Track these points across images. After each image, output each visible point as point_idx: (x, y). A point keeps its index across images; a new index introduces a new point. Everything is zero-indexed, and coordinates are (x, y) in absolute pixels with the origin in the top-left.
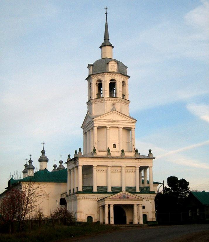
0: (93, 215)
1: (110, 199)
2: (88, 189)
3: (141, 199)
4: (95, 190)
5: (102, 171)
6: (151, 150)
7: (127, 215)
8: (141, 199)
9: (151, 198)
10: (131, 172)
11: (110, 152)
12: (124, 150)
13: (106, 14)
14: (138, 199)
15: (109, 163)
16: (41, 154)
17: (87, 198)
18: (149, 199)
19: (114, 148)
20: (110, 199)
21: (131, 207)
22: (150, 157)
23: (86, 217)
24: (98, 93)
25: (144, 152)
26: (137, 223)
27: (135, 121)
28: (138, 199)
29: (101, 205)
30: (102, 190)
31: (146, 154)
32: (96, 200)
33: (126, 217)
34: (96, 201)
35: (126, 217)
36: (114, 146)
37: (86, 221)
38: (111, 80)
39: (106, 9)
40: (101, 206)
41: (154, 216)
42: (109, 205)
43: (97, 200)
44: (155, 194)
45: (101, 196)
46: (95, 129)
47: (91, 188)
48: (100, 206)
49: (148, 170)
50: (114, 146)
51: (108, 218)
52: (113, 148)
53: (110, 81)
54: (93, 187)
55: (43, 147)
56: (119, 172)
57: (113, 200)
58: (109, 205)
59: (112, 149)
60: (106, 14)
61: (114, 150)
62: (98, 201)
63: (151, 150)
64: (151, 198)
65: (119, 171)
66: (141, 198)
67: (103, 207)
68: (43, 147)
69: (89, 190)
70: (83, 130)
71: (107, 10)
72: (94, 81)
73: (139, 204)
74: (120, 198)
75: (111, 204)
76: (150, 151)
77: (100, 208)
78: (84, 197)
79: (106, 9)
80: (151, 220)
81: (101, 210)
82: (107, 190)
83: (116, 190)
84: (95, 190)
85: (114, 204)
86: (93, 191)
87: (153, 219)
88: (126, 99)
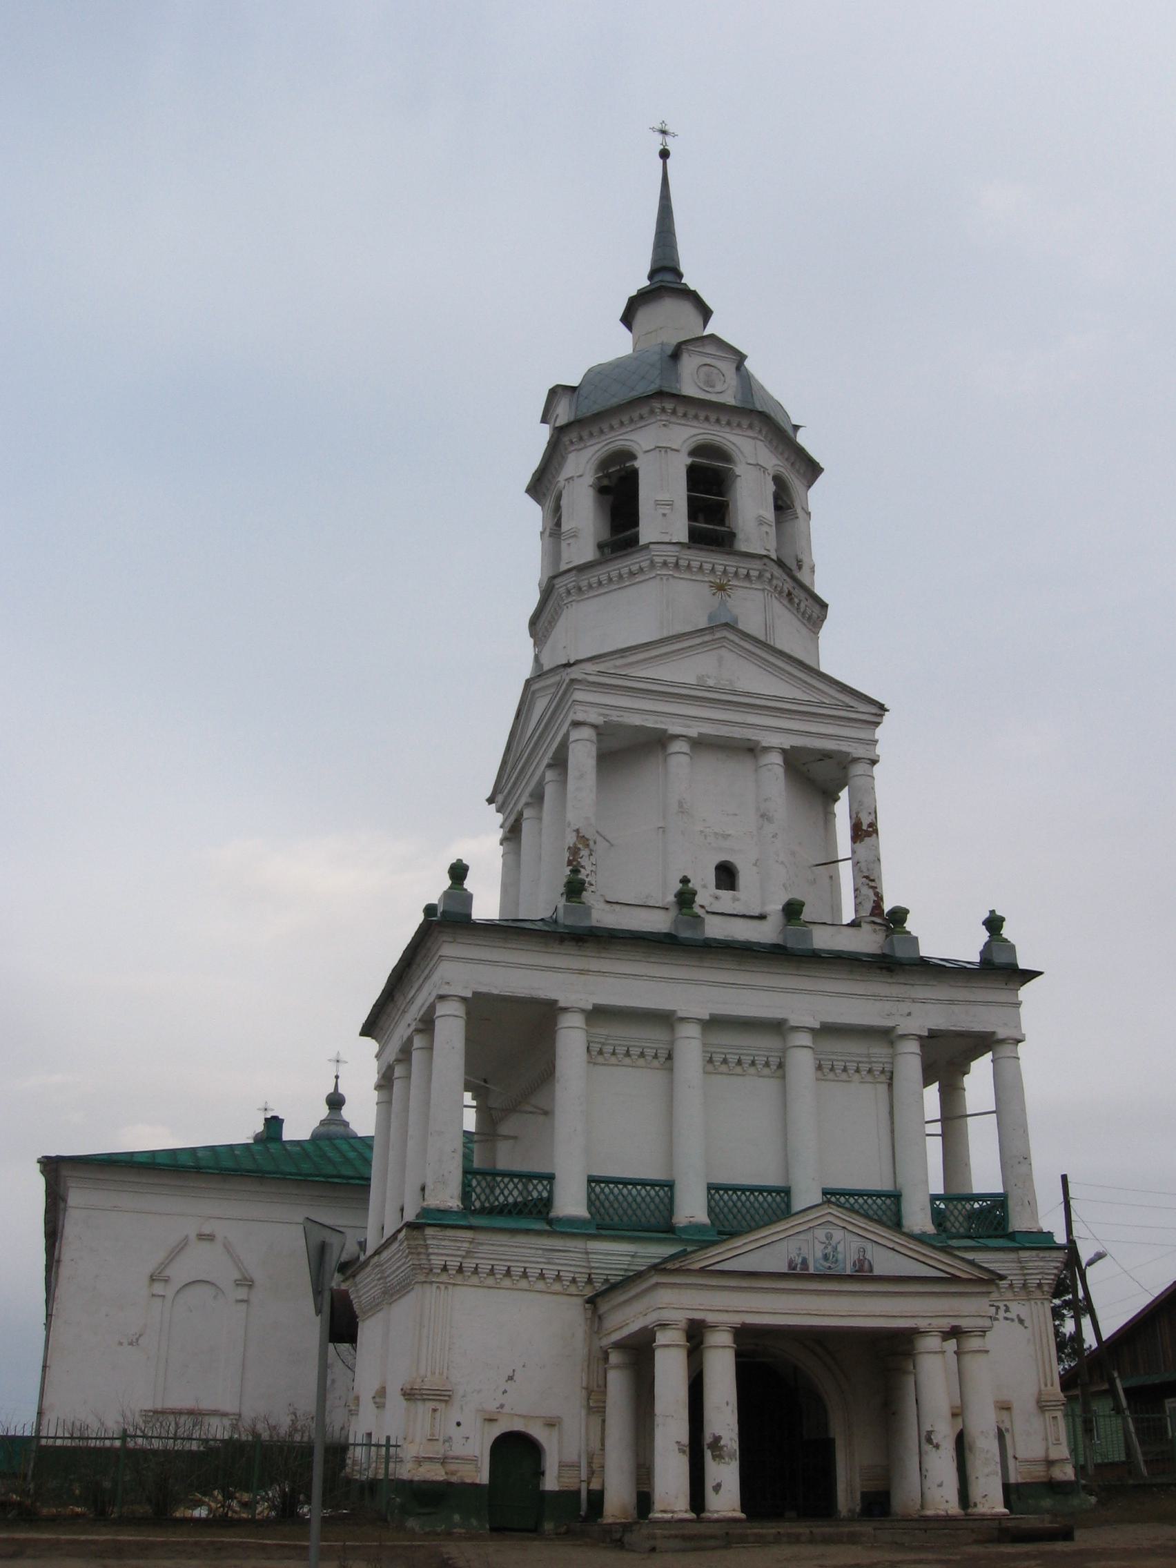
0: (551, 1424)
1: (703, 1271)
2: (511, 1193)
3: (980, 1281)
4: (571, 1202)
5: (628, 1054)
6: (1002, 919)
7: (837, 1431)
8: (980, 1281)
9: (1025, 1286)
10: (857, 1076)
11: (697, 909)
12: (802, 904)
13: (664, 154)
14: (954, 1279)
15: (693, 993)
16: (324, 1111)
17: (501, 1268)
18: (1009, 1295)
19: (726, 894)
20: (703, 1271)
21: (889, 1353)
22: (1000, 970)
23: (518, 1426)
24: (605, 535)
25: (947, 936)
26: (953, 1508)
27: (874, 710)
28: (954, 1279)
29: (616, 1337)
30: (633, 1209)
31: (967, 947)
32: (573, 1290)
33: (826, 1448)
34: (579, 1301)
35: (833, 1440)
36: (726, 875)
37: (484, 1477)
38: (696, 451)
39: (664, 132)
40: (618, 1345)
41: (1057, 1442)
42: (696, 1334)
43: (589, 1292)
44: (1055, 1254)
45: (615, 1255)
46: (583, 755)
47: (537, 1191)
48: (606, 1342)
49: (979, 1079)
50: (726, 875)
51: (681, 1456)
52: (720, 892)
53: (692, 453)
54: (551, 1178)
55: (337, 1077)
56: (766, 1071)
57: (733, 1283)
58: (696, 1334)
59: (707, 894)
60: (664, 154)
61: (726, 900)
62: (592, 1301)
63: (1002, 919)
64: (1025, 1286)
65: (767, 1064)
66: (977, 1273)
67: (639, 1352)
68: (337, 1077)
69: (516, 1204)
70: (500, 818)
71: (669, 139)
72: (581, 469)
73: (964, 1323)
74: (797, 1275)
75: (711, 1318)
76: (994, 924)
77: (606, 1359)
78: (469, 1264)
79: (664, 132)
80: (1039, 1473)
81: (617, 1384)
82: (671, 1211)
83: (748, 1208)
84: (571, 1202)
85: (737, 1320)
86: (552, 1214)
87: (1050, 1463)
88: (779, 646)
